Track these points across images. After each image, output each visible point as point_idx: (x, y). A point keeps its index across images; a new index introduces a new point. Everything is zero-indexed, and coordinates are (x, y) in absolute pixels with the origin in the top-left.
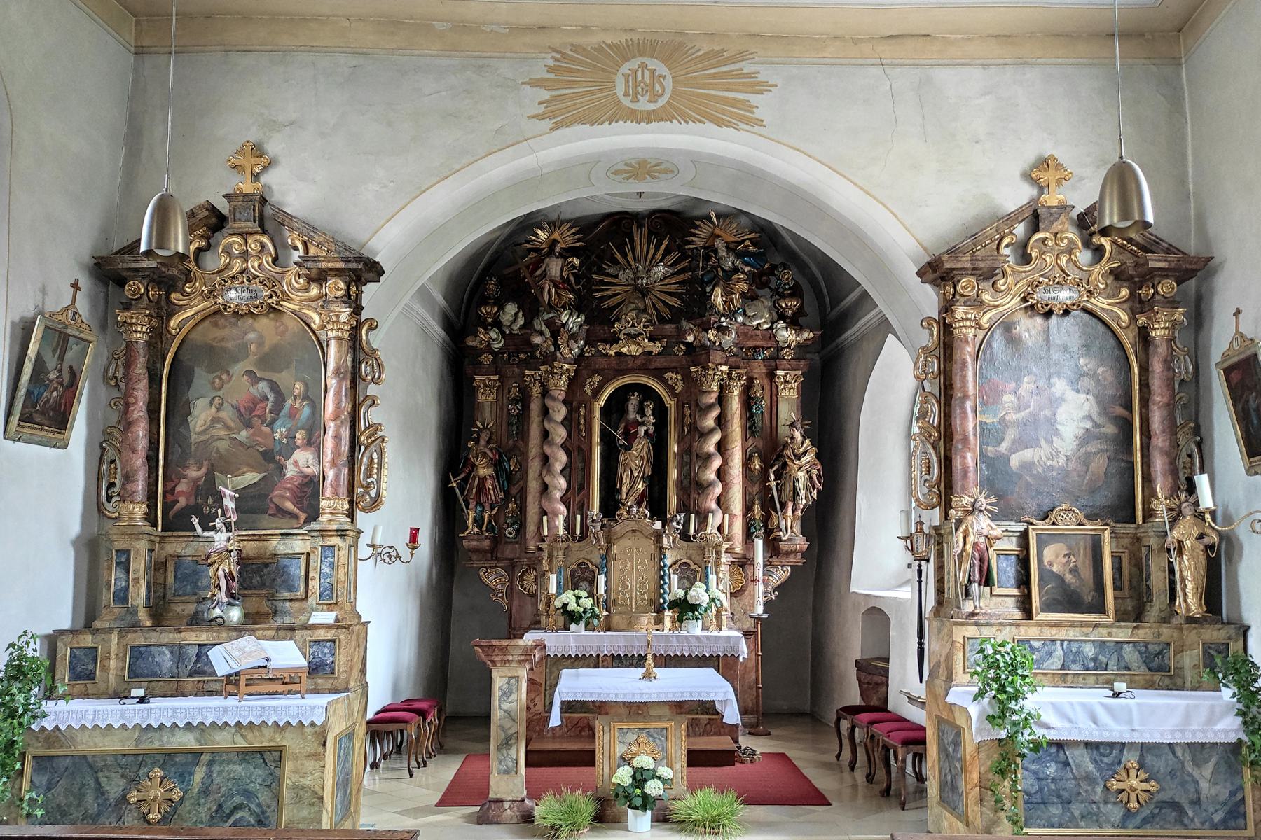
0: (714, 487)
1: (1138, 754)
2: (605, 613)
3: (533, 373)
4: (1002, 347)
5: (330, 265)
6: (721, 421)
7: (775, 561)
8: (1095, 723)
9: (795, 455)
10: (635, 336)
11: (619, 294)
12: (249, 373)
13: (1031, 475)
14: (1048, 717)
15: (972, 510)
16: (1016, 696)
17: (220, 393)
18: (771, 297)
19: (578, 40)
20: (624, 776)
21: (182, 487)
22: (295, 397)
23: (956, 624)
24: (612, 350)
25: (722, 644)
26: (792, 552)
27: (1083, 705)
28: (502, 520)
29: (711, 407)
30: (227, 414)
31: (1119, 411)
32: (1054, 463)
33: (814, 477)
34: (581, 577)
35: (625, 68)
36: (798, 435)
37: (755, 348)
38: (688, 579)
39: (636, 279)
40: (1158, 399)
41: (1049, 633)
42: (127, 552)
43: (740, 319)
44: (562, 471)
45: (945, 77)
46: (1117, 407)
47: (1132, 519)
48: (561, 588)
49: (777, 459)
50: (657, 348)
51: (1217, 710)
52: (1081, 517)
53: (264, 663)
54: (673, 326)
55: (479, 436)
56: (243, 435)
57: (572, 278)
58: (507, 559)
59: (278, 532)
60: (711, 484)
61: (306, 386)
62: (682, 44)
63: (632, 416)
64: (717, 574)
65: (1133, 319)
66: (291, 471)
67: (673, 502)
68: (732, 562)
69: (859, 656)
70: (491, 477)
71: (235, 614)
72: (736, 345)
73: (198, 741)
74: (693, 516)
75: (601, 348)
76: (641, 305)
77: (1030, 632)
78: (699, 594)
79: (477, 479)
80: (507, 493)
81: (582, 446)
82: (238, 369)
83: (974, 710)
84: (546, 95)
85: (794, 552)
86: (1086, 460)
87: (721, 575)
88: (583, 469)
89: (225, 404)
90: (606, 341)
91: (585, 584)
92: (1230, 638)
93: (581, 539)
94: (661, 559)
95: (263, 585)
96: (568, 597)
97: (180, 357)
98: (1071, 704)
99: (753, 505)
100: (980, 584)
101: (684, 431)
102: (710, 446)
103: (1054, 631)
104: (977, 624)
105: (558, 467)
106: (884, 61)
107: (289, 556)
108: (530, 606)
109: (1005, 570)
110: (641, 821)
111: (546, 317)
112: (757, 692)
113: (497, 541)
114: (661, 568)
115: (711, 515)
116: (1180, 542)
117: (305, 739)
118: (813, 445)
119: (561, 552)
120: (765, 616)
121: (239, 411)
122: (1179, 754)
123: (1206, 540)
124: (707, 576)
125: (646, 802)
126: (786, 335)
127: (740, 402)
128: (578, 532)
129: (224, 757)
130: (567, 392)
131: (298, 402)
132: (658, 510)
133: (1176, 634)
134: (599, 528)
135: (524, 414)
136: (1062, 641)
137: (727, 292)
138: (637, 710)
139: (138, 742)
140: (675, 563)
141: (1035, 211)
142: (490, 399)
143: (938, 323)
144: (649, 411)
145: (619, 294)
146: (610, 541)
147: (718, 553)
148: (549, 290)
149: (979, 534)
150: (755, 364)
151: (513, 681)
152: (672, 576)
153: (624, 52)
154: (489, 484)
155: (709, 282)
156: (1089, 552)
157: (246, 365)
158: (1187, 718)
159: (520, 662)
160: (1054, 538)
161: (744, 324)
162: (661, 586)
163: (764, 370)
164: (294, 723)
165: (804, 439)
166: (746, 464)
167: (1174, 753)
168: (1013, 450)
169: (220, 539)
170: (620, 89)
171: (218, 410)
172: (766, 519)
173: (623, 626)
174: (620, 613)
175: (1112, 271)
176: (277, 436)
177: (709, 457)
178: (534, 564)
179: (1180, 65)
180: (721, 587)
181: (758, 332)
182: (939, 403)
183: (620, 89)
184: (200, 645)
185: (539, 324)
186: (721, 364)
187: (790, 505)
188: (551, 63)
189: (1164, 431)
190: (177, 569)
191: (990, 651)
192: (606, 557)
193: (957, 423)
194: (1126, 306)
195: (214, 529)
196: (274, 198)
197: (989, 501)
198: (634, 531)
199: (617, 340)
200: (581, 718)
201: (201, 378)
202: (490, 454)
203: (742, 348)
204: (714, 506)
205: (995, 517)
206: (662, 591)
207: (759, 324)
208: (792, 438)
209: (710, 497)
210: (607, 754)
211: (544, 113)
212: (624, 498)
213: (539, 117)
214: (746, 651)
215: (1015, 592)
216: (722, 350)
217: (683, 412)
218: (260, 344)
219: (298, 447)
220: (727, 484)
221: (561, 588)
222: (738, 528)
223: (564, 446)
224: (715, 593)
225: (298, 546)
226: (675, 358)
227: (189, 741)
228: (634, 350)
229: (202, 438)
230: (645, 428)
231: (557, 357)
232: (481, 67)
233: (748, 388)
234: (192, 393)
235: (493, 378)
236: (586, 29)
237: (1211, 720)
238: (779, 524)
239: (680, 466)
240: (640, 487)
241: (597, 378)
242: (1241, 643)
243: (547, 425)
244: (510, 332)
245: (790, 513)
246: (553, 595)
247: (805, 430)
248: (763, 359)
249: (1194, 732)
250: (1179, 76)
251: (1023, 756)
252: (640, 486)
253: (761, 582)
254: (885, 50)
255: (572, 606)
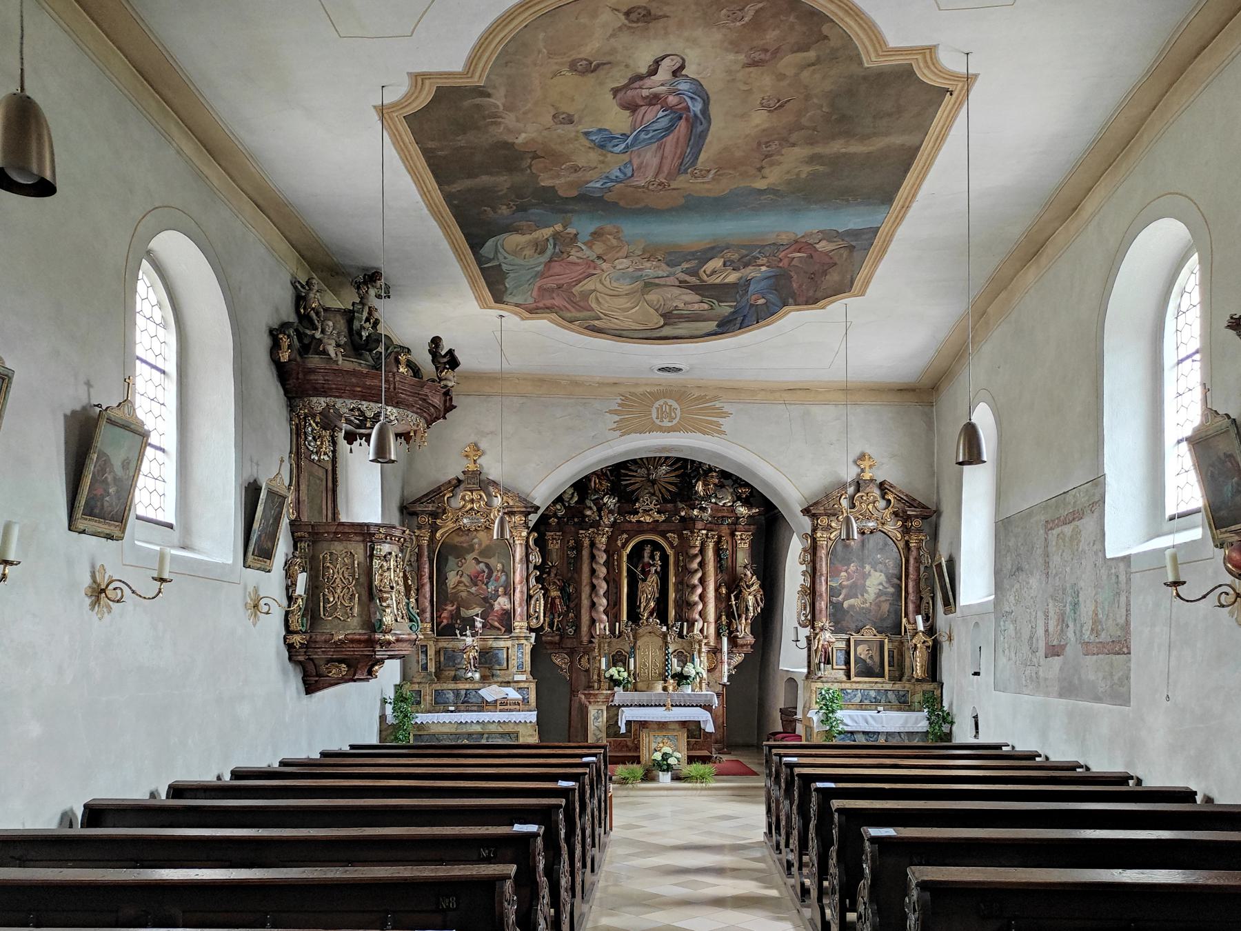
0: (698, 605)
1: (885, 737)
2: (634, 681)
3: (584, 532)
4: (841, 549)
5: (518, 510)
6: (702, 565)
7: (734, 649)
8: (867, 723)
9: (747, 586)
10: (649, 511)
11: (637, 482)
12: (475, 559)
13: (853, 612)
14: (846, 721)
15: (822, 629)
16: (833, 711)
17: (461, 569)
18: (732, 486)
19: (633, 390)
20: (658, 756)
21: (445, 614)
22: (498, 571)
23: (813, 682)
24: (634, 519)
25: (703, 699)
26: (745, 645)
27: (862, 716)
28: (565, 624)
29: (696, 556)
30: (465, 579)
31: (896, 581)
32: (864, 606)
33: (759, 599)
34: (618, 659)
35: (657, 405)
36: (748, 573)
37: (723, 517)
38: (682, 661)
39: (649, 474)
40: (912, 577)
41: (855, 686)
42: (426, 646)
43: (713, 500)
44: (604, 594)
45: (816, 410)
46: (895, 579)
47: (901, 634)
48: (608, 667)
49: (736, 588)
50: (663, 518)
51: (919, 718)
52: (875, 632)
53: (506, 696)
54: (672, 505)
55: (550, 571)
56: (473, 589)
57: (608, 472)
58: (568, 648)
59: (493, 637)
60: (696, 604)
61: (503, 566)
62: (685, 392)
63: (646, 559)
64: (700, 658)
65: (903, 536)
66: (497, 607)
67: (672, 613)
68: (708, 651)
69: (782, 707)
70: (559, 597)
71: (477, 676)
72: (711, 516)
73: (482, 729)
74: (685, 624)
75: (627, 518)
76: (652, 491)
77: (847, 686)
78: (690, 670)
79: (550, 599)
80: (568, 607)
81: (616, 579)
82: (470, 557)
83: (815, 718)
84: (617, 418)
85: (746, 645)
86: (879, 605)
87: (702, 659)
88: (616, 593)
89: (464, 574)
90: (630, 513)
91: (620, 664)
92: (935, 689)
93: (619, 637)
94: (667, 649)
95: (486, 663)
96: (613, 671)
97: (441, 551)
98: (857, 715)
99: (721, 616)
100: (824, 663)
101: (679, 570)
102: (695, 581)
103: (857, 685)
104: (822, 682)
105: (602, 592)
106: (786, 402)
107: (498, 649)
108: (583, 677)
109: (838, 657)
110: (665, 778)
111: (594, 498)
112: (723, 729)
113: (563, 636)
114: (667, 654)
115: (696, 623)
116: (915, 645)
117: (527, 728)
118: (758, 579)
119: (606, 645)
120: (728, 683)
121: (471, 578)
122: (902, 737)
123: (926, 644)
124: (693, 660)
125: (669, 768)
126: (742, 510)
127: (713, 551)
128: (617, 633)
129: (493, 735)
130: (606, 545)
131: (499, 573)
132: (664, 619)
133: (912, 687)
134: (629, 631)
135: (579, 557)
136: (861, 690)
137: (705, 485)
138: (662, 726)
139: (457, 729)
140: (675, 651)
141: (858, 482)
142: (556, 547)
143: (810, 537)
144: (657, 558)
145: (637, 482)
146: (635, 638)
147: (700, 646)
148: (595, 481)
149: (825, 640)
150: (723, 527)
151: (600, 712)
152: (673, 659)
153: (656, 396)
154: (557, 601)
155: (694, 477)
156: (878, 648)
157: (474, 555)
158: (906, 721)
159: (603, 702)
160: (862, 642)
161: (716, 503)
162: (667, 665)
163: (728, 531)
164: (523, 722)
165: (753, 576)
166: (717, 590)
167: (900, 737)
168: (844, 600)
169: (469, 640)
170: (654, 416)
171: (461, 577)
172: (729, 625)
173: (644, 689)
174: (643, 681)
175: (894, 512)
176: (490, 590)
177: (694, 587)
178: (588, 651)
179: (933, 406)
180: (702, 666)
181: (724, 508)
182: (810, 576)
183: (654, 416)
184: (466, 690)
185: (589, 503)
186: (702, 529)
187: (744, 616)
188: (620, 401)
189: (913, 592)
190: (445, 654)
191: (823, 692)
192: (634, 647)
193: (818, 587)
194: (899, 530)
195: (466, 635)
196: (485, 470)
197: (830, 625)
198: (650, 633)
199: (637, 513)
200: (621, 741)
201: (452, 561)
202: (558, 583)
203: (714, 517)
204: (697, 617)
205: (833, 632)
206: (667, 668)
207: (725, 503)
208: (745, 575)
209: (696, 611)
210: (647, 748)
211: (617, 427)
212: (642, 611)
213: (614, 430)
214: (717, 702)
215: (844, 667)
216: (703, 520)
217: (678, 558)
218: (480, 545)
219: (500, 596)
220: (705, 603)
221: (608, 667)
222: (712, 630)
223: (605, 579)
224: (700, 669)
225: (502, 644)
226: (673, 524)
227: (478, 729)
228: (648, 519)
229: (453, 591)
230: (655, 568)
231: (600, 523)
232: (585, 403)
233: (718, 543)
234: (447, 569)
235: (558, 534)
236: (637, 385)
237: (917, 722)
238: (737, 627)
239: (677, 591)
240: (652, 604)
241: (625, 536)
242: (940, 690)
243: (594, 566)
244: (569, 505)
245: (744, 621)
246: (603, 670)
247: (753, 570)
248: (727, 524)
249: (908, 727)
250: (932, 412)
251: (835, 737)
252: (652, 604)
253: (726, 663)
254: (786, 396)
255: (616, 676)
